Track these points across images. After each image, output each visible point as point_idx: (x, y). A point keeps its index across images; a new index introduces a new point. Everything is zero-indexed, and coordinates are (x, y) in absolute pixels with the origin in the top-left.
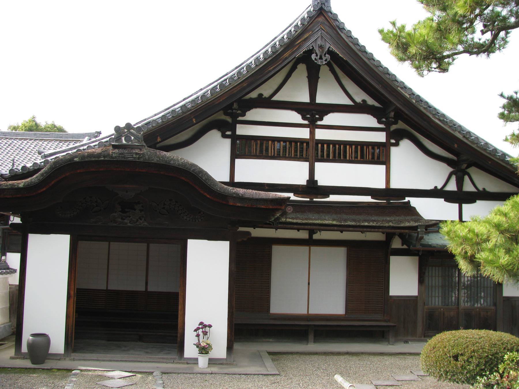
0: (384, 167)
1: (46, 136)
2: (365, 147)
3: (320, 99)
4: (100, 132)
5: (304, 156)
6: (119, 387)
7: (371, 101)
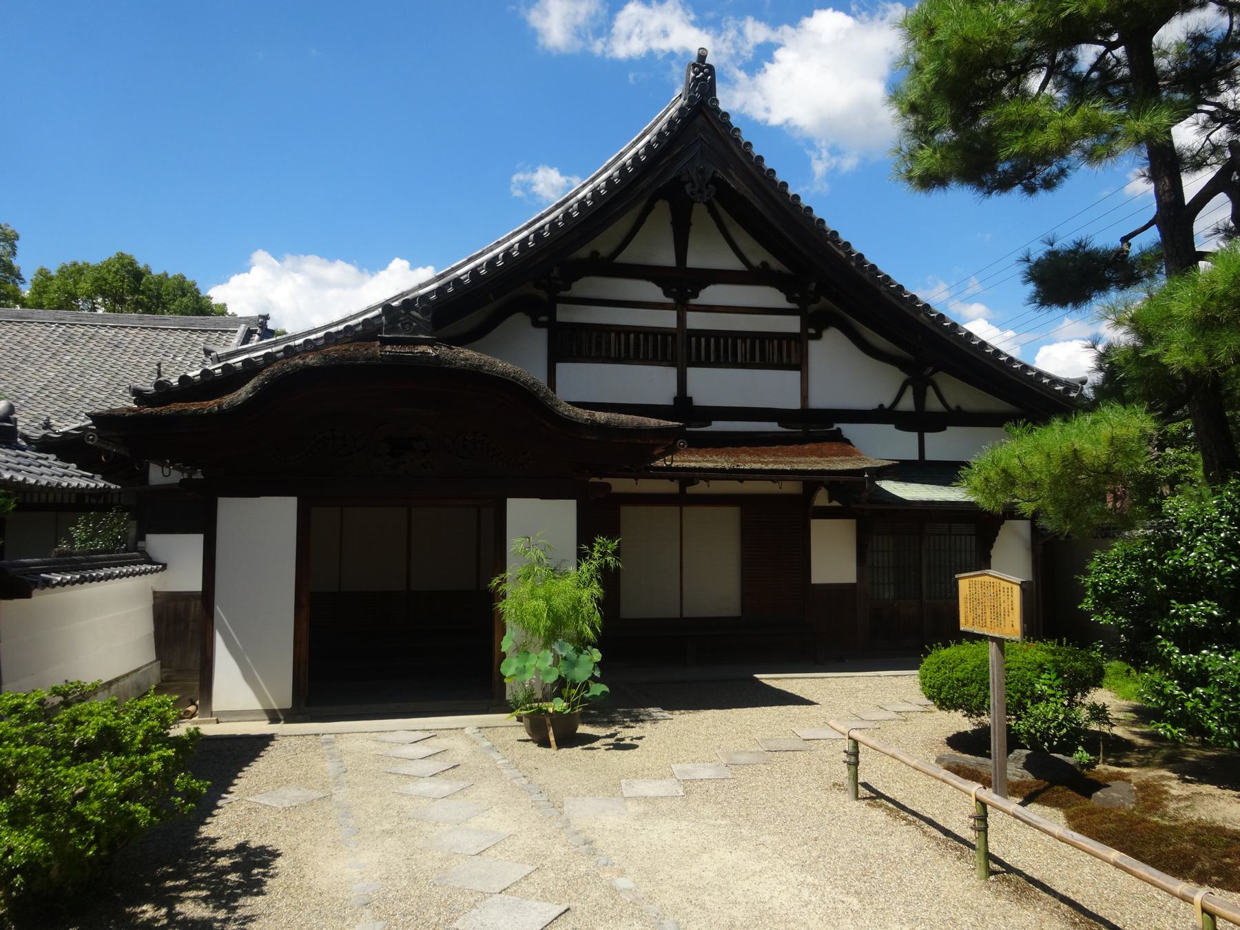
0: (797, 374)
1: (163, 322)
2: (767, 342)
3: (693, 261)
4: (268, 315)
5: (669, 357)
6: (416, 742)
7: (775, 264)
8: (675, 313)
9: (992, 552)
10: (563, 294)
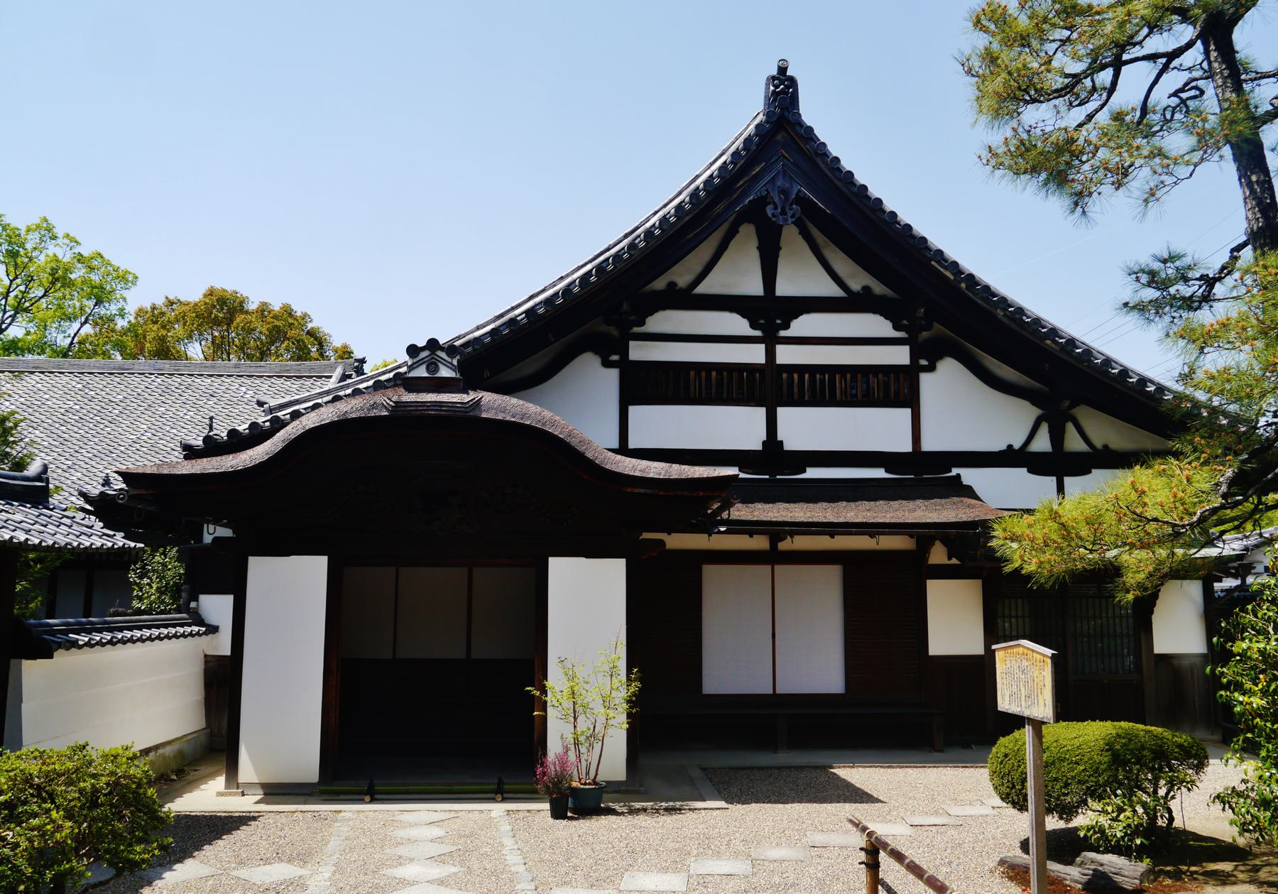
4: (364, 358)
7: (878, 288)
8: (763, 346)
9: (1154, 618)
10: (636, 330)
